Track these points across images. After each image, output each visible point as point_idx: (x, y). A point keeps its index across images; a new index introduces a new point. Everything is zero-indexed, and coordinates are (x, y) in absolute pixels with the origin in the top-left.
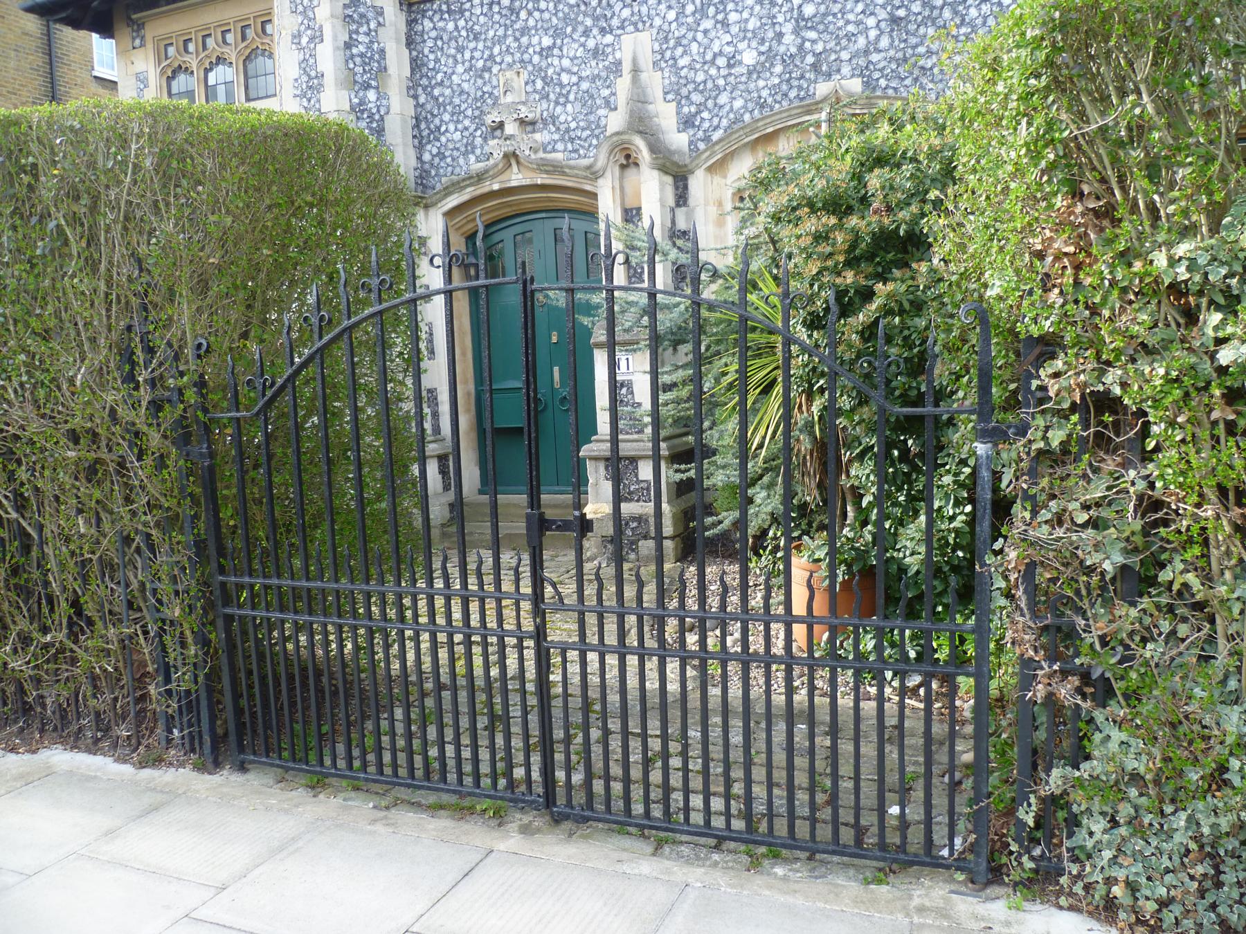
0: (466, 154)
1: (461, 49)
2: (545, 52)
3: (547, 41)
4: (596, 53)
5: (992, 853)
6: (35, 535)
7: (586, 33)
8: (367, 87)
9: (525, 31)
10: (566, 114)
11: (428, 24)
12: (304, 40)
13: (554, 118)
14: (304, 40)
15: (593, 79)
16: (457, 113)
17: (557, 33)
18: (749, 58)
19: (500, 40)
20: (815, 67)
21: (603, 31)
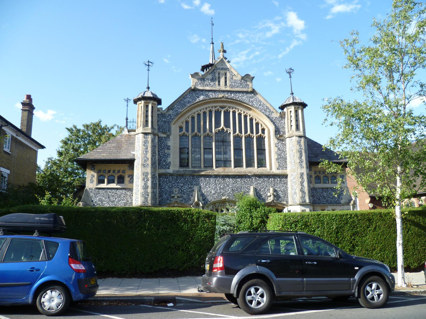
0: (167, 200)
1: (167, 184)
2: (182, 186)
3: (182, 185)
4: (190, 188)
5: (268, 117)
6: (353, 198)
7: (189, 185)
8: (155, 188)
9: (178, 183)
10: (185, 196)
11: (161, 179)
12: (145, 180)
13: (183, 197)
14: (145, 180)
15: (189, 191)
16: (166, 194)
17: (184, 184)
18: (213, 192)
19: (174, 183)
20: (222, 194)
21: (191, 185)
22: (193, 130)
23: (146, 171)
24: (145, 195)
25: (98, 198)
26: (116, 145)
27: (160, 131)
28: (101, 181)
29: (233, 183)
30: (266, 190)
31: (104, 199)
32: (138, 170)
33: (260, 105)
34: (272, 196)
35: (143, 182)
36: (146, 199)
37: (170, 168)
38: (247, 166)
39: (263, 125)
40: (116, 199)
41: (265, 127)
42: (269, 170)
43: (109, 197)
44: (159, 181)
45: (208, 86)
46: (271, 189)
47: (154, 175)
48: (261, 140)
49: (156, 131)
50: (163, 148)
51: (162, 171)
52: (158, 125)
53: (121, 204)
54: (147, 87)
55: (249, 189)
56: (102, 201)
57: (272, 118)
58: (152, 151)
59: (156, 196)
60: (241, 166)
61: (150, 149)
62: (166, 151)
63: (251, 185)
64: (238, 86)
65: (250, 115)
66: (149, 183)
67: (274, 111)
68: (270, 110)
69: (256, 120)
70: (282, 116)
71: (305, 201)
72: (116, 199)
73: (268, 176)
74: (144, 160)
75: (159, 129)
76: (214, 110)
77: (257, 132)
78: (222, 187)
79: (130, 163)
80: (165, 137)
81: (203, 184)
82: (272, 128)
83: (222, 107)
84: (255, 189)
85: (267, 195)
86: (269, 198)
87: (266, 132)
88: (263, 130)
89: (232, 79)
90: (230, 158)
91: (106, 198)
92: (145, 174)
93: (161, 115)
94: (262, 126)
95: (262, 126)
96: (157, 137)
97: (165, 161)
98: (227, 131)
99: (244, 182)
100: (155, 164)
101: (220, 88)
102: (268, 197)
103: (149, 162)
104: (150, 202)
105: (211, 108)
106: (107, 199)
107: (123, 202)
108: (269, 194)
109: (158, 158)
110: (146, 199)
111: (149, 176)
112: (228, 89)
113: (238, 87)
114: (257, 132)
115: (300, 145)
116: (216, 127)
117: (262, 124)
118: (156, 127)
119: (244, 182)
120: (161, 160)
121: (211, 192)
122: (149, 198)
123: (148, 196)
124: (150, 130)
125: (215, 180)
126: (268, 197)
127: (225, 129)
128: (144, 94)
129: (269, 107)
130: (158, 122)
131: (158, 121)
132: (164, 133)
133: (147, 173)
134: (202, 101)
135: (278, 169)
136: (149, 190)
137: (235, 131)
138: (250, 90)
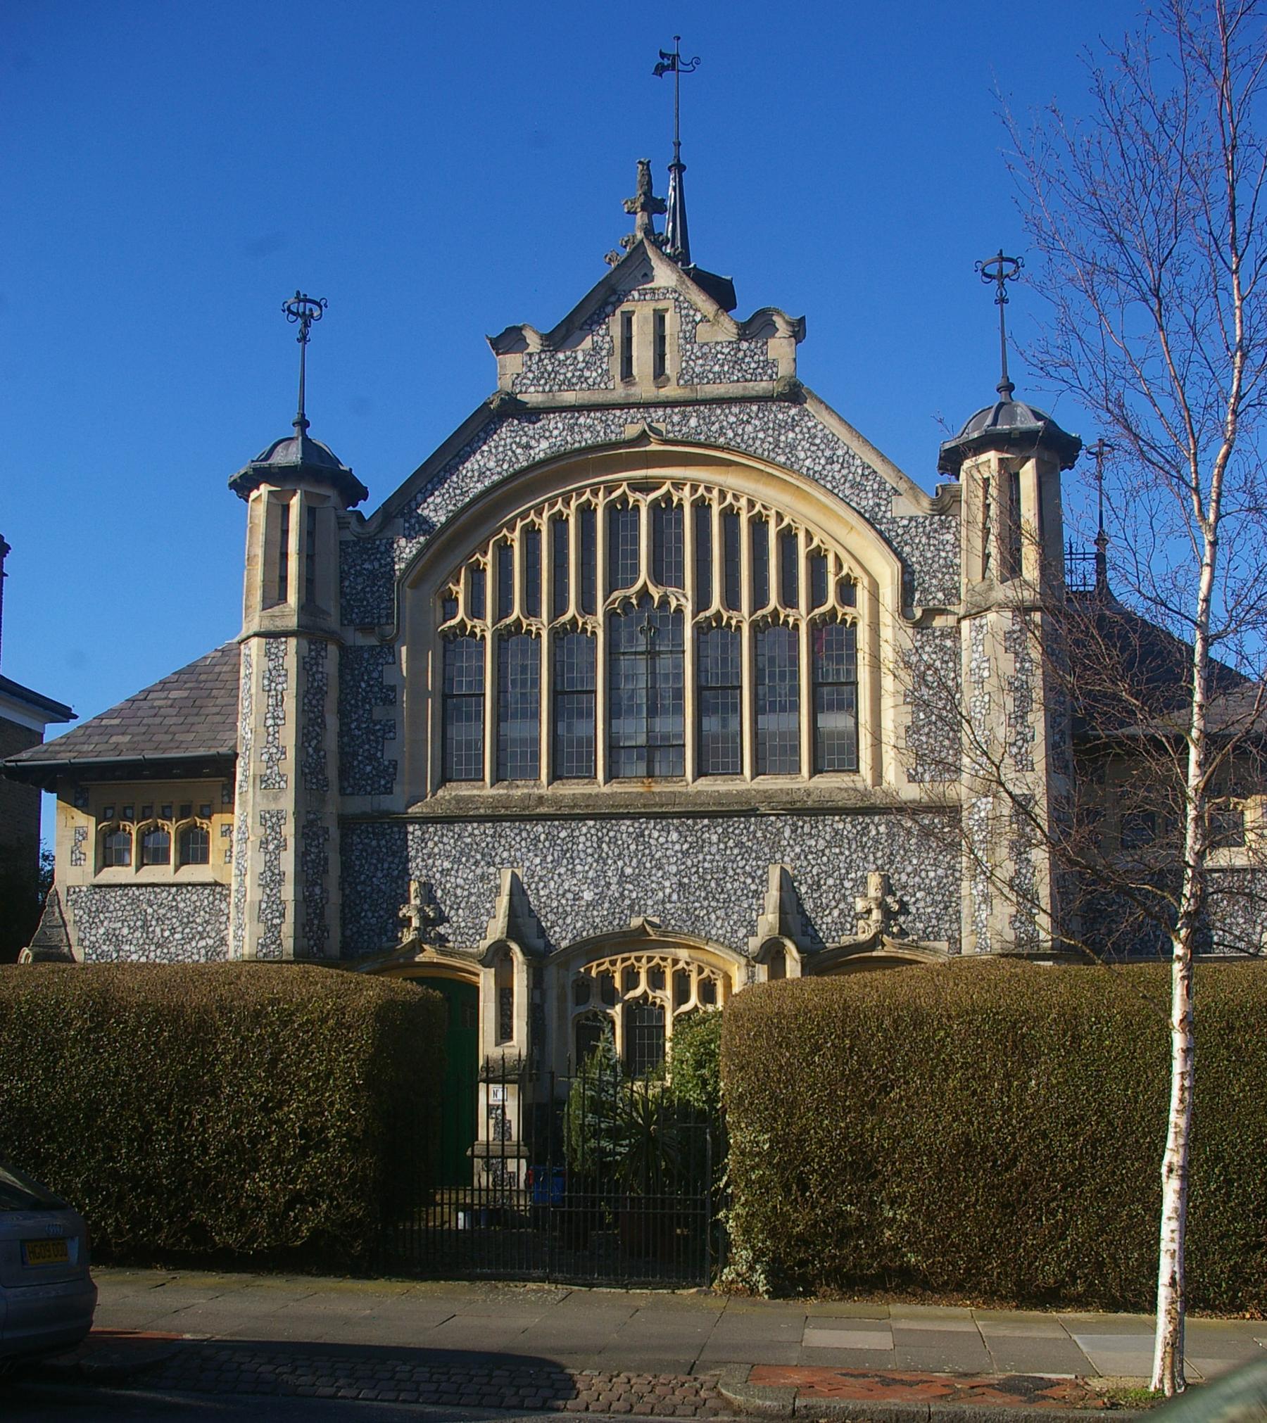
1: (381, 861)
3: (447, 865)
7: (476, 863)
12: (271, 847)
14: (271, 847)
18: (588, 896)
20: (631, 907)
21: (488, 864)
22: (503, 608)
23: (273, 807)
24: (269, 913)
25: (102, 931)
26: (185, 694)
27: (351, 622)
28: (108, 855)
29: (685, 854)
30: (848, 884)
31: (125, 931)
32: (248, 803)
33: (830, 461)
34: (876, 915)
35: (262, 857)
36: (273, 929)
37: (396, 789)
38: (497, 779)
39: (848, 563)
40: (173, 931)
41: (857, 572)
42: (869, 782)
43: (145, 926)
44: (344, 850)
45: (571, 386)
46: (874, 880)
47: (311, 823)
48: (834, 639)
49: (333, 622)
50: (364, 700)
51: (360, 804)
52: (342, 594)
53: (195, 953)
54: (296, 417)
55: (764, 882)
56: (113, 938)
57: (893, 521)
58: (302, 711)
59: (321, 916)
60: (796, 769)
61: (290, 705)
62: (378, 713)
63: (771, 860)
64: (718, 375)
65: (780, 517)
66: (288, 862)
67: (902, 486)
68: (882, 483)
69: (809, 537)
70: (945, 504)
71: (277, 940)
72: (173, 931)
73: (864, 810)
74: (265, 757)
75: (345, 612)
76: (600, 502)
77: (817, 597)
78: (628, 871)
79: (224, 766)
80: (372, 648)
81: (544, 859)
82: (886, 572)
83: (644, 487)
84: (787, 883)
85: (852, 907)
86: (861, 923)
87: (862, 595)
88: (847, 590)
89: (691, 340)
90: (682, 735)
91: (133, 929)
92: (270, 821)
93: (355, 544)
94: (839, 565)
95: (839, 565)
96: (333, 649)
97: (371, 758)
98: (664, 602)
99: (740, 844)
100: (322, 771)
101: (633, 390)
102: (858, 917)
103: (289, 765)
104: (289, 944)
105: (587, 495)
106: (138, 934)
107: (203, 943)
108: (860, 905)
109: (341, 747)
110: (273, 929)
111: (289, 830)
112: (671, 391)
113: (718, 377)
114: (817, 597)
115: (1021, 657)
116: (610, 588)
117: (844, 555)
118: (330, 604)
119: (740, 844)
120: (355, 754)
121: (577, 897)
122: (288, 928)
123: (283, 915)
124: (295, 619)
125: (600, 840)
126: (858, 917)
127: (656, 593)
128: (269, 454)
129: (877, 465)
130: (342, 582)
131: (343, 576)
132: (366, 629)
133: (279, 816)
134: (542, 463)
135: (912, 779)
136: (288, 892)
137: (702, 601)
138: (779, 388)
